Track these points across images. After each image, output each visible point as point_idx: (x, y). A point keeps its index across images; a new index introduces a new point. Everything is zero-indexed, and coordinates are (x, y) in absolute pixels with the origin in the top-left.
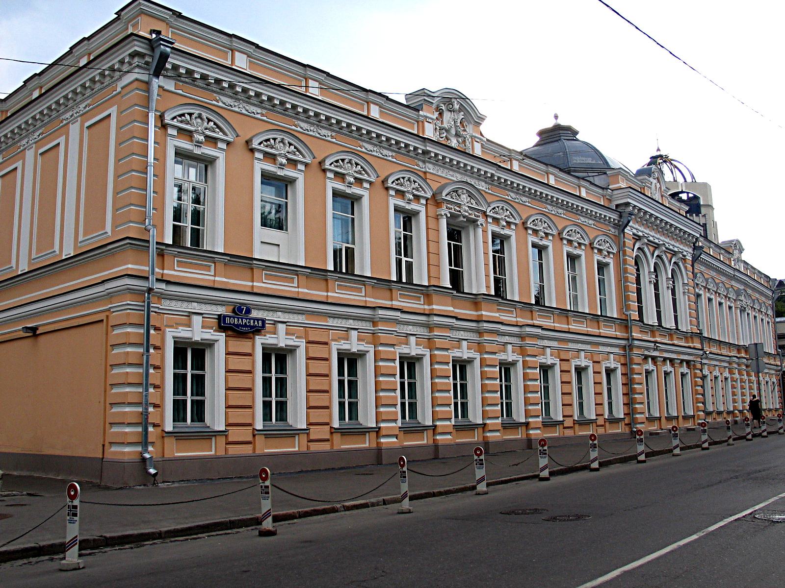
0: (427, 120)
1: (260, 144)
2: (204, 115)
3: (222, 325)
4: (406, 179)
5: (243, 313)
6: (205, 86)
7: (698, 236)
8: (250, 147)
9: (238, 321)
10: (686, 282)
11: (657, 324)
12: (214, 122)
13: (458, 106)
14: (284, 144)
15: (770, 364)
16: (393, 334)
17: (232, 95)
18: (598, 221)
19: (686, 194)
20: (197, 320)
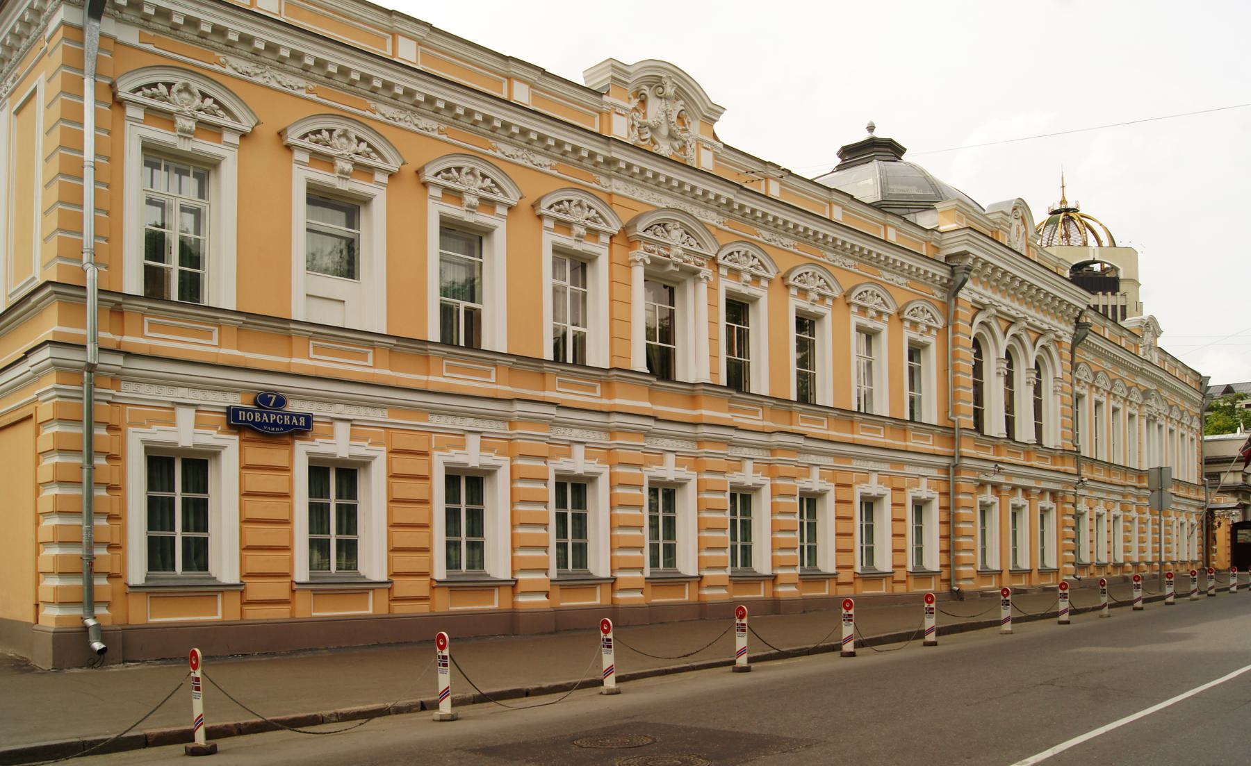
0: (704, 146)
1: (551, 207)
3: (235, 421)
4: (810, 274)
5: (271, 405)
7: (1084, 307)
8: (285, 143)
9: (261, 417)
10: (1059, 375)
11: (1006, 436)
13: (673, 90)
15: (1190, 499)
16: (639, 450)
17: (575, 161)
18: (913, 279)
19: (1099, 264)
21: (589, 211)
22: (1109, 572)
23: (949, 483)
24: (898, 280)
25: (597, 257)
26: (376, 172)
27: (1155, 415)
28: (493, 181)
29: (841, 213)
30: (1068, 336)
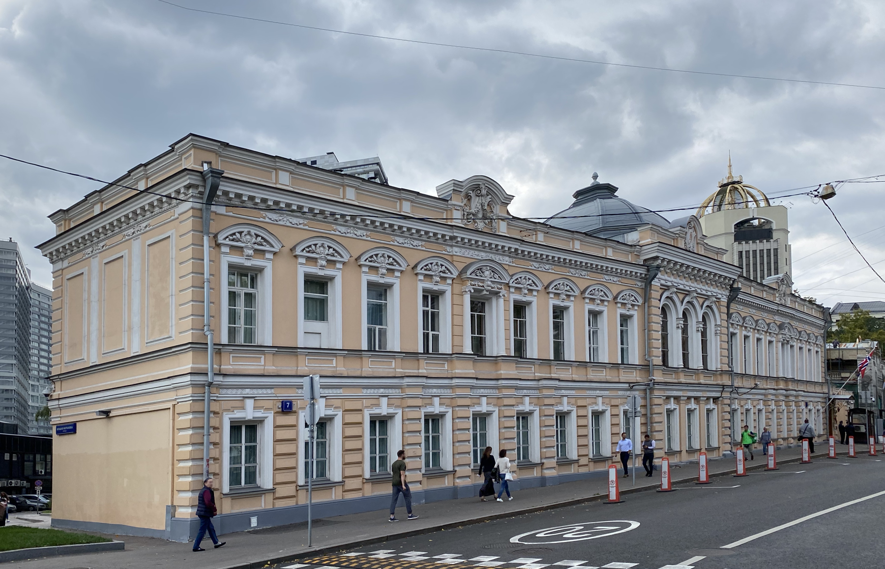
1: (225, 239)
2: (253, 232)
6: (312, 217)
10: (719, 323)
11: (683, 367)
12: (333, 249)
14: (324, 247)
18: (623, 277)
22: (755, 446)
23: (646, 399)
24: (614, 279)
27: (788, 339)
28: (393, 259)
29: (543, 236)
30: (725, 297)
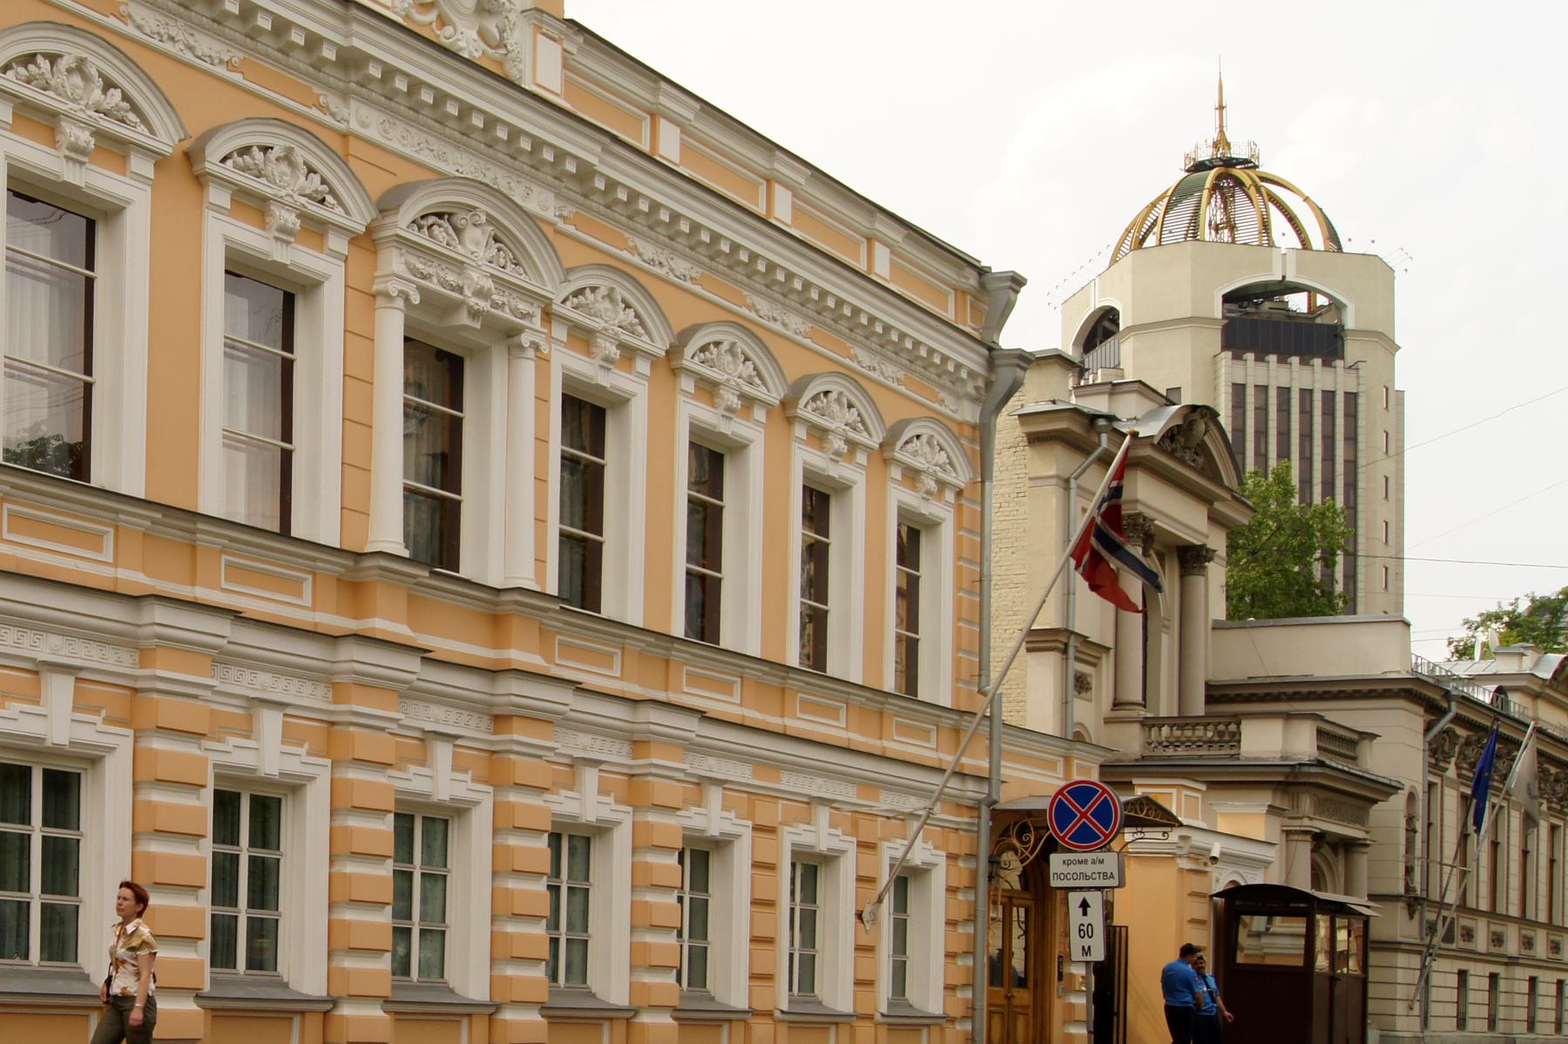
0: (544, 30)
2: (95, 65)
20: (271, 722)
21: (744, 362)
25: (122, 209)
26: (683, 376)
28: (126, 97)
